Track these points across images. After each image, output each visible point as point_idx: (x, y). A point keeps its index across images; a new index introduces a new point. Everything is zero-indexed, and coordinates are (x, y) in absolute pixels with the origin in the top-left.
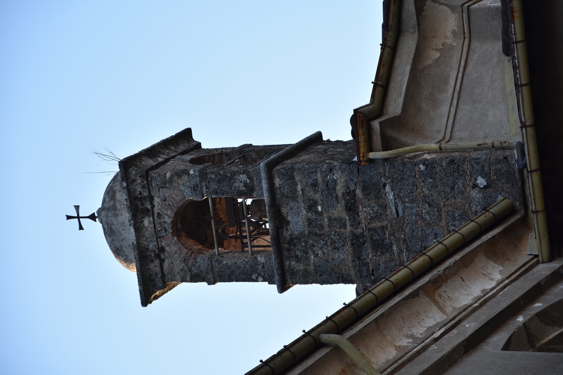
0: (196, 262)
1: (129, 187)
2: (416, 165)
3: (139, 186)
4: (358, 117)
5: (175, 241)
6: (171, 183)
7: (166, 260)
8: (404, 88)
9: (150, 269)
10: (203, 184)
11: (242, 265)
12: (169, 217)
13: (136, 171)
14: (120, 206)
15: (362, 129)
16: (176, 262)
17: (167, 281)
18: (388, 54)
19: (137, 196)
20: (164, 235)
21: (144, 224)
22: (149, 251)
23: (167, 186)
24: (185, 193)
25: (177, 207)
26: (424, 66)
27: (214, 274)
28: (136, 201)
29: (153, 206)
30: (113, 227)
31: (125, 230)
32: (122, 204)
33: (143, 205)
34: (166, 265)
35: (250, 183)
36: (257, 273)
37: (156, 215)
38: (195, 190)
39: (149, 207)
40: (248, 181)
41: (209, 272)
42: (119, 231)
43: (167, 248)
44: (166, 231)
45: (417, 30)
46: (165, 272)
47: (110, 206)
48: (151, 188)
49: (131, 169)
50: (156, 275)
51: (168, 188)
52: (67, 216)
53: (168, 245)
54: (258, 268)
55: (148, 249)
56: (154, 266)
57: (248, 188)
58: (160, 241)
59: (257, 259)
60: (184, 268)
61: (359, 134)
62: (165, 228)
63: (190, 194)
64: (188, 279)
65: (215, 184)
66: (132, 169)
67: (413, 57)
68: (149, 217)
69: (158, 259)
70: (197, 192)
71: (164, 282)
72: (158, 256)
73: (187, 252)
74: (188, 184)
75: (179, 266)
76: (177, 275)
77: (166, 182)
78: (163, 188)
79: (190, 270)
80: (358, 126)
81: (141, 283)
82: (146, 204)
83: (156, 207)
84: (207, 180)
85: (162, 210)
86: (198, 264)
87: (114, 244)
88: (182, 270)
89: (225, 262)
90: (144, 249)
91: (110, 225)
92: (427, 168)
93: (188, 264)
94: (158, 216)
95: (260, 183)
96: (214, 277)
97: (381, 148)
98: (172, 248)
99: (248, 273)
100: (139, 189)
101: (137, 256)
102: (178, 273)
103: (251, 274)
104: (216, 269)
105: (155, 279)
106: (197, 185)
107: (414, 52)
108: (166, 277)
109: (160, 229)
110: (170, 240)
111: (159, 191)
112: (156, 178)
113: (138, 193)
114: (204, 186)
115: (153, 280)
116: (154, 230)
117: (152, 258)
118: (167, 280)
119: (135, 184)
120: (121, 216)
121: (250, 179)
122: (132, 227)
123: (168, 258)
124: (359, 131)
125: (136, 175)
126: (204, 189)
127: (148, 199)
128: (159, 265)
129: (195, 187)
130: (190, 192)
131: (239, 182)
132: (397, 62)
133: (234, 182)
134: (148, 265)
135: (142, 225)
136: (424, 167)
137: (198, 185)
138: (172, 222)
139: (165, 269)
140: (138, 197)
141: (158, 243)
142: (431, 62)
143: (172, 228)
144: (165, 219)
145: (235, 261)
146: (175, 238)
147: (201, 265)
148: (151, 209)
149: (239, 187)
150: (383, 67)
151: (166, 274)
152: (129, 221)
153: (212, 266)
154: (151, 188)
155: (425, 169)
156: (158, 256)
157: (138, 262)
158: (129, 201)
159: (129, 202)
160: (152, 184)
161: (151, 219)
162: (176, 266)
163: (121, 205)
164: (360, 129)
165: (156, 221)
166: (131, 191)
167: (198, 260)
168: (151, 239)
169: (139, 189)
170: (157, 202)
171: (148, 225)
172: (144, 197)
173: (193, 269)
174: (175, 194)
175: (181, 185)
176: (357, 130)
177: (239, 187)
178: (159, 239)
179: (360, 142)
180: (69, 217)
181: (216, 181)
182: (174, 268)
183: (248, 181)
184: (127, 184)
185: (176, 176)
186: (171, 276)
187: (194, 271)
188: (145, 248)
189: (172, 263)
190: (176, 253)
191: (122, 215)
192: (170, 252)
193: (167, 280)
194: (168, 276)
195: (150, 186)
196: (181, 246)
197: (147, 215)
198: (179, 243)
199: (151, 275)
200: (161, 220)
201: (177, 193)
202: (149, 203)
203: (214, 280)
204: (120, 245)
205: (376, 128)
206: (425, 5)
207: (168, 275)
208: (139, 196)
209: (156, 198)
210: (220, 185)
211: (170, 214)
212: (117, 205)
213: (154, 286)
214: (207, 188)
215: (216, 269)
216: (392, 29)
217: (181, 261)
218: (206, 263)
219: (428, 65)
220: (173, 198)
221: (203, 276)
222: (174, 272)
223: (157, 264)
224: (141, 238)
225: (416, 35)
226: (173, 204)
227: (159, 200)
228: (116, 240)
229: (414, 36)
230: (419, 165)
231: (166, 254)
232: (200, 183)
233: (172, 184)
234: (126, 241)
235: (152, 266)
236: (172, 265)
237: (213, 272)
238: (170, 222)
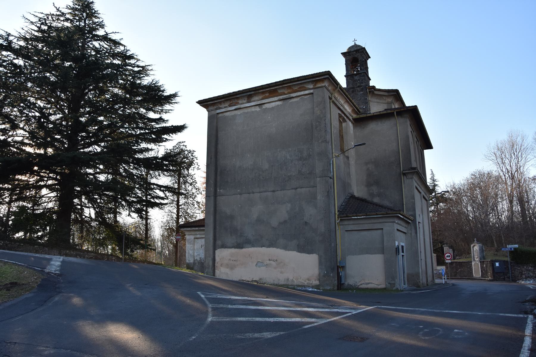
34: (348, 56)
72: (349, 55)
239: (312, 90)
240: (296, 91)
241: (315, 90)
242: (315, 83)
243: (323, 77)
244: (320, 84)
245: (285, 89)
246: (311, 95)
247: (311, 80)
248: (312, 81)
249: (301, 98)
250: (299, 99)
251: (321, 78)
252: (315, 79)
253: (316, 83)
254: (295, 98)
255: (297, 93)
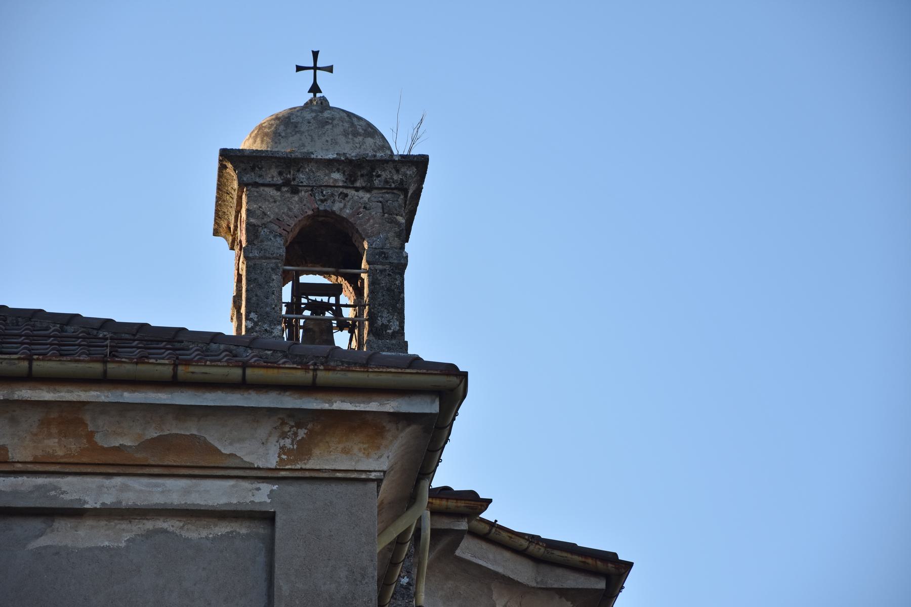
0: (275, 237)
1: (391, 162)
2: (408, 572)
3: (389, 176)
4: (482, 503)
5: (306, 212)
6: (390, 221)
7: (279, 193)
8: (481, 562)
9: (270, 169)
10: (387, 266)
11: (269, 301)
12: (341, 210)
13: (410, 176)
14: (358, 142)
15: (464, 506)
16: (277, 207)
17: (249, 189)
18: (521, 545)
19: (376, 171)
20: (315, 197)
21: (334, 172)
22: (296, 173)
23: (386, 215)
24: (375, 239)
25: (355, 224)
26: (493, 588)
27: (258, 259)
28: (369, 168)
29: (357, 189)
30: (329, 127)
31: (327, 143)
32: (361, 146)
33: (362, 176)
34: (272, 192)
35: (386, 333)
36: (259, 321)
37: (345, 191)
38: (381, 254)
39: (358, 184)
40: (390, 331)
41: (262, 252)
42: (324, 134)
43: (296, 198)
44: (322, 201)
45: (539, 586)
46: (262, 188)
47: (356, 127)
48: (383, 191)
49: (416, 169)
50: (260, 176)
51: (383, 216)
52: (318, 52)
53: (301, 200)
54: (265, 323)
55: (298, 171)
56: (273, 175)
57: (380, 330)
58: (307, 189)
59: (279, 324)
60: (267, 216)
61: (459, 501)
62: (326, 200)
63: (374, 246)
64: (251, 221)
65: (386, 283)
66: (414, 171)
67: (512, 577)
68: (343, 181)
69: (283, 183)
70: (377, 257)
71: (247, 185)
72: (287, 183)
73: (289, 226)
74: (388, 245)
75: (270, 211)
76: (257, 204)
77: (392, 214)
78: (383, 208)
79: (264, 225)
80: (470, 502)
81: (255, 154)
82: (362, 180)
83: (356, 193)
84: (393, 273)
85: (351, 202)
86: (272, 238)
87: (302, 123)
88: (264, 214)
89: (274, 278)
90: (300, 166)
91: (331, 123)
92: (403, 587)
93: (273, 224)
94: (344, 193)
95: (388, 348)
96: (254, 258)
97: (434, 527)
98: (297, 205)
99: (259, 309)
100: (384, 175)
101: (293, 155)
102: (260, 207)
103: (257, 312)
104: (265, 264)
105: (255, 173)
106: (386, 258)
107: (516, 579)
108: (255, 189)
109: (324, 192)
110: (308, 205)
111: (377, 202)
112: (397, 201)
113: (379, 172)
114: (384, 267)
115: (253, 169)
116: (324, 184)
117: (284, 175)
118: (250, 189)
119: (394, 171)
120: (345, 141)
121: (392, 335)
122: (335, 156)
123: (281, 196)
124: (463, 502)
125: (405, 175)
126: (380, 267)
127: (369, 184)
128: (273, 182)
129: (385, 255)
130: (377, 247)
131: (388, 319)
132: (507, 555)
133: (389, 311)
134: (277, 167)
135: (334, 169)
136: (405, 584)
137: (386, 259)
138: (333, 212)
139: (267, 189)
140: (374, 172)
141: (305, 186)
142: (494, 597)
143: (325, 211)
144: (339, 203)
145: (275, 292)
146: (310, 213)
147: (272, 243)
148: (355, 185)
149: (382, 317)
150: (509, 536)
151: (257, 190)
152: (344, 153)
153: (269, 258)
154: (383, 191)
155: (402, 585)
156: (287, 183)
157: (285, 156)
158: (373, 159)
159: (371, 159)
160: (388, 193)
161: (341, 184)
162: (270, 206)
163: (359, 143)
164: (465, 503)
165: (336, 189)
166: (385, 165)
167: (278, 239)
168: (311, 177)
169: (385, 175)
170: (363, 196)
171: (333, 178)
172: (372, 181)
173: (265, 230)
174: (374, 224)
175: (387, 235)
176: (465, 500)
177: (382, 317)
178: (310, 189)
179: (448, 502)
180: (315, 54)
181: (391, 286)
182: (267, 203)
183: (390, 331)
184: (396, 161)
185: (399, 230)
186: (255, 196)
187: (263, 231)
188: (300, 168)
189: (275, 202)
190: (290, 209)
191: (347, 142)
192: (291, 200)
193: (250, 189)
194: (255, 192)
195: (386, 191)
196: (300, 219)
197: (347, 179)
198: (303, 216)
199: (261, 169)
200: (337, 197)
201: (376, 227)
202: (364, 185)
203: (250, 257)
204: (303, 132)
205: (459, 525)
206: (568, 600)
207: (257, 192)
208: (374, 174)
209: (368, 195)
210: (385, 290)
211: (345, 212)
212: (359, 137)
213: (245, 169)
214: (382, 271)
215: (265, 264)
216: (548, 553)
217: (277, 214)
218: (276, 251)
219: (492, 595)
220: (369, 220)
221: (255, 242)
222: (261, 201)
223: (275, 179)
224: (317, 165)
225: (534, 584)
226: (359, 218)
227: (366, 199)
228: (310, 128)
229: (532, 581)
230: (408, 578)
231: (288, 195)
232: (390, 262)
233: (388, 222)
234: (310, 143)
235: (274, 172)
236: (271, 200)
237: (261, 258)
238: (334, 209)
239: (266, 488)
240: (110, 459)
241: (292, 489)
242: (302, 433)
243: (392, 405)
244: (346, 451)
245: (14, 421)
246: (242, 529)
247: (290, 401)
248: (293, 413)
249: (150, 534)
250: (127, 536)
251: (373, 406)
252: (326, 406)
253: (311, 434)
254: (89, 522)
255: (118, 480)
